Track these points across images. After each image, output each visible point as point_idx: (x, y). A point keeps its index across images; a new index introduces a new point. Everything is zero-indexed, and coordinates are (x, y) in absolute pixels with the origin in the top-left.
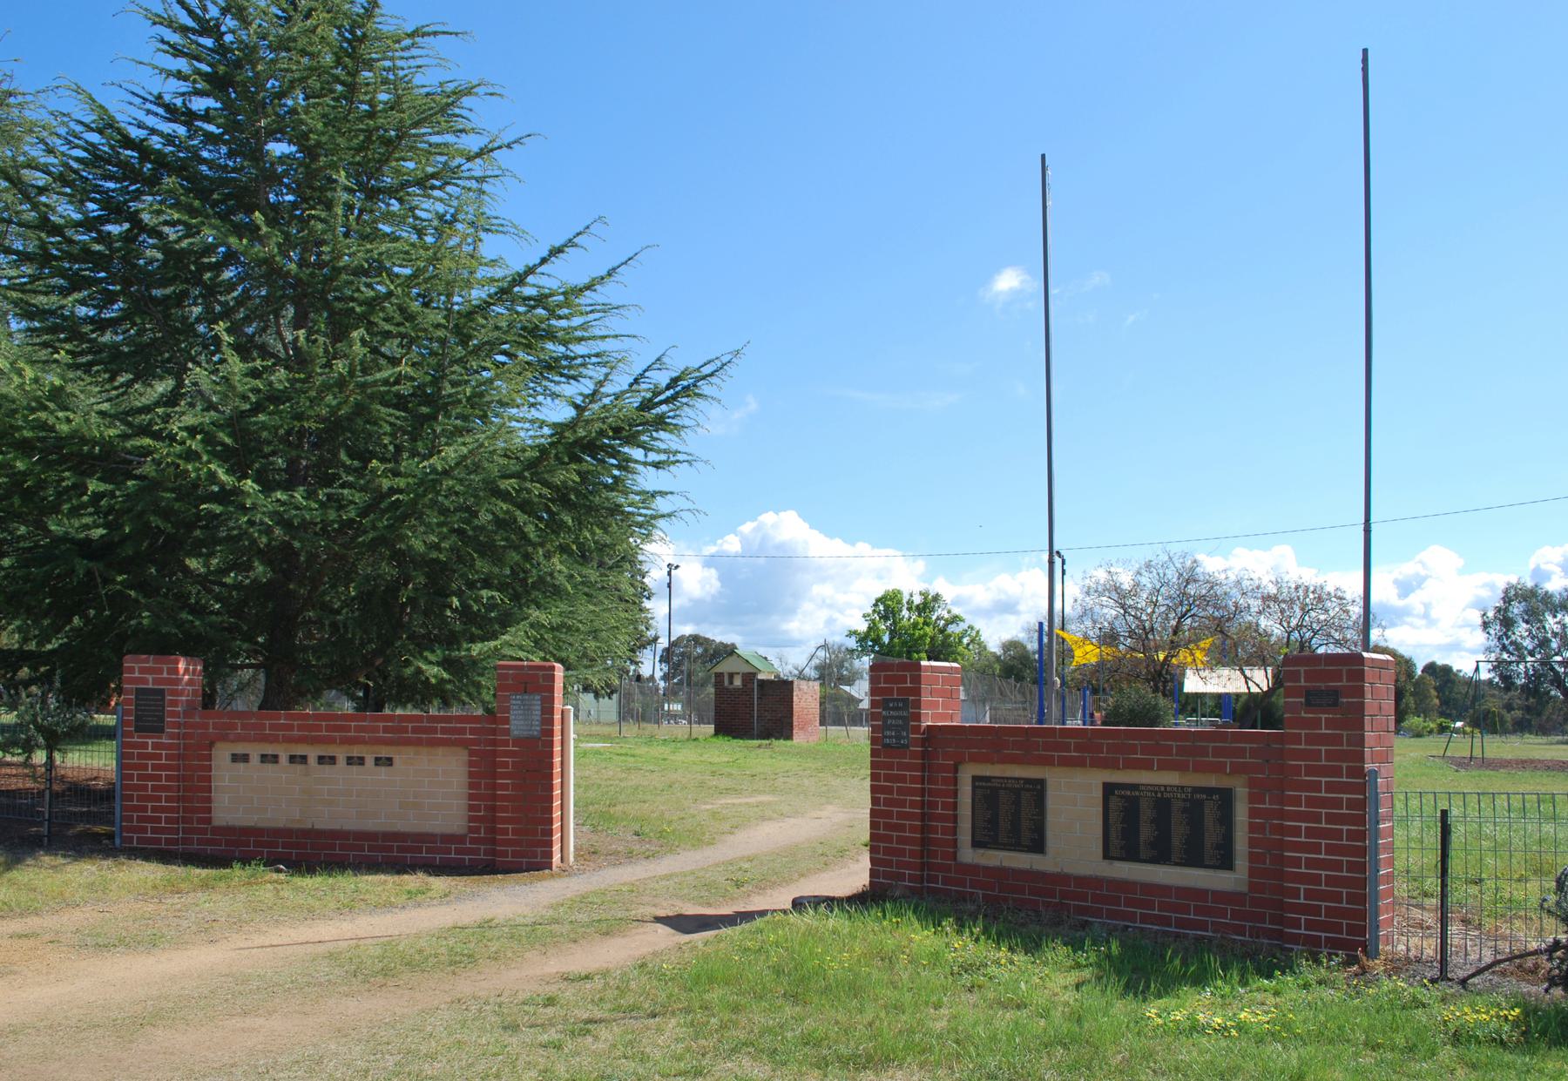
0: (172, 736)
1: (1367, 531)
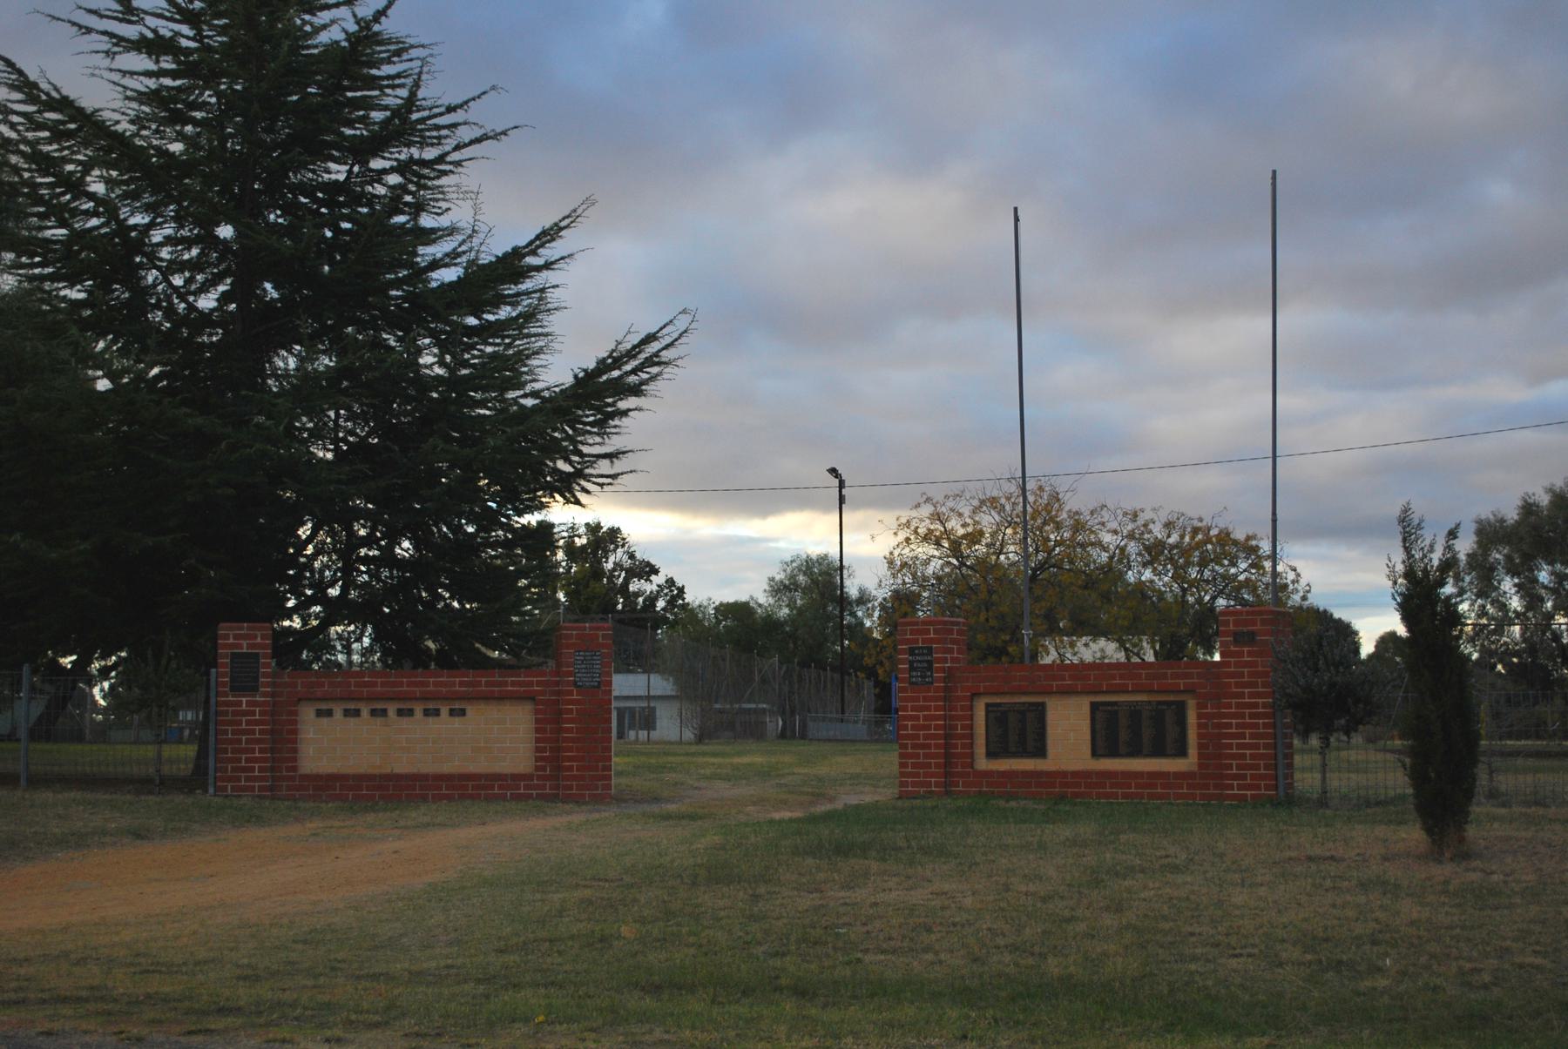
0: (265, 694)
1: (1274, 521)
